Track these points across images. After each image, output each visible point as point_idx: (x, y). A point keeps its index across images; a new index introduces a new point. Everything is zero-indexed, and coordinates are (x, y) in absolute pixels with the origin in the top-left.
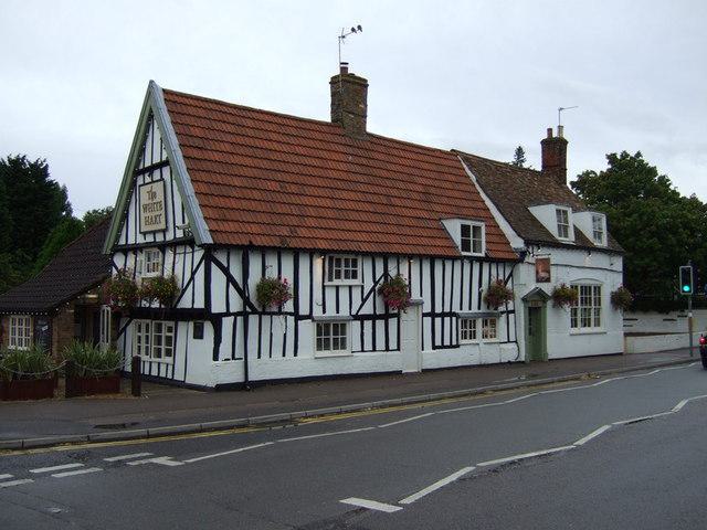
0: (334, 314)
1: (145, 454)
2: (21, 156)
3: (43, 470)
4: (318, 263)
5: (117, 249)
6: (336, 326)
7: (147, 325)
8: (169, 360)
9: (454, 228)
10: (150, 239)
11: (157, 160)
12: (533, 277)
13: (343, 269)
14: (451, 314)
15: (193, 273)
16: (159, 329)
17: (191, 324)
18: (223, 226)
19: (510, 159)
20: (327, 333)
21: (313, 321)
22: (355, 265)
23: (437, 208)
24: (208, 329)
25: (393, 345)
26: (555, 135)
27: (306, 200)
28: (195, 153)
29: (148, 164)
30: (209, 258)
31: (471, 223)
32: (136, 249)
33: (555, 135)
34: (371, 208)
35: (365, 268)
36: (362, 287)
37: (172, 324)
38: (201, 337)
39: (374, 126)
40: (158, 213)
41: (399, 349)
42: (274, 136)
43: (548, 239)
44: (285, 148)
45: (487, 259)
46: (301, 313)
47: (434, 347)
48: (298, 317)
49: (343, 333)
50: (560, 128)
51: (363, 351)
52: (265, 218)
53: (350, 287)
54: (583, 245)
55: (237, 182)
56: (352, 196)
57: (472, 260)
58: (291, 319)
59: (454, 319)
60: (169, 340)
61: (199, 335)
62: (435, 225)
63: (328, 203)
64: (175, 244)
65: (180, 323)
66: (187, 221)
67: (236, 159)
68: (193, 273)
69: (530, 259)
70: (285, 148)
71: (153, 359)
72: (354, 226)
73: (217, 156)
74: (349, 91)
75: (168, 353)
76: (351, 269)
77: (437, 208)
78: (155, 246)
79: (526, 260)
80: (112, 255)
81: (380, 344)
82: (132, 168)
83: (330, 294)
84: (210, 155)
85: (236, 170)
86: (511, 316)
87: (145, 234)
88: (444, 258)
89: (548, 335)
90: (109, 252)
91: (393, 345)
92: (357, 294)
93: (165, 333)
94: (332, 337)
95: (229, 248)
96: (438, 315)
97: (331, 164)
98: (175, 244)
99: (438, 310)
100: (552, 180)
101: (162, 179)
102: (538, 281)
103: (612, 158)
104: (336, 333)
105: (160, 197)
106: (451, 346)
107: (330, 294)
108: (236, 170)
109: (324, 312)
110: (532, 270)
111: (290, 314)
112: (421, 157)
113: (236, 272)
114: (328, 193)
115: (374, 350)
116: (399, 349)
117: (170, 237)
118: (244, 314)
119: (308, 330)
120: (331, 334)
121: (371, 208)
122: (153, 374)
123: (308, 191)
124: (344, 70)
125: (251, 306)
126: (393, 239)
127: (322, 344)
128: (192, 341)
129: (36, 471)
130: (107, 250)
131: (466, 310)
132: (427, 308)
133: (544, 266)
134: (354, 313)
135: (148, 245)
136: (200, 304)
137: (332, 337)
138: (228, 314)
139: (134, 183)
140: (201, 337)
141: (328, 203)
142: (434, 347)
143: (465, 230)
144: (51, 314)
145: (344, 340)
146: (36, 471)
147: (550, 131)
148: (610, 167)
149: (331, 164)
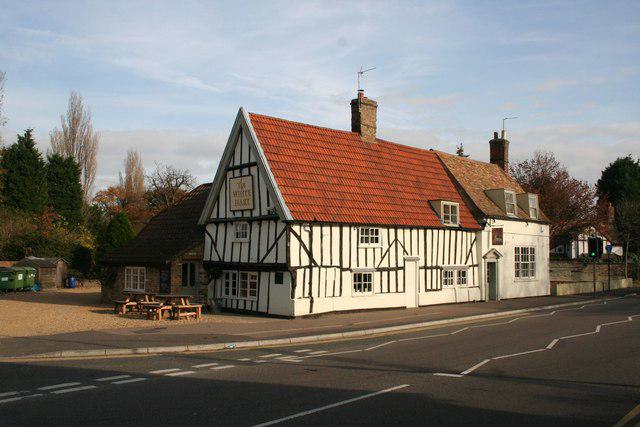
2: (22, 135)
3: (104, 379)
4: (354, 232)
5: (209, 221)
7: (234, 275)
8: (255, 299)
10: (239, 215)
11: (245, 161)
14: (437, 267)
15: (277, 240)
16: (244, 277)
17: (273, 275)
18: (298, 208)
19: (340, 120)
20: (360, 280)
21: (351, 271)
22: (377, 233)
25: (400, 288)
26: (500, 137)
28: (274, 158)
29: (237, 163)
32: (226, 222)
35: (383, 232)
37: (256, 273)
42: (319, 144)
45: (460, 229)
46: (344, 266)
47: (427, 290)
48: (342, 270)
50: (503, 132)
56: (372, 185)
57: (451, 229)
58: (338, 270)
60: (253, 285)
61: (279, 280)
64: (260, 220)
66: (272, 205)
68: (277, 240)
73: (287, 159)
75: (253, 293)
78: (244, 220)
80: (205, 226)
81: (393, 288)
82: (224, 165)
83: (362, 252)
84: (283, 159)
86: (400, 272)
87: (234, 212)
91: (400, 288)
92: (378, 251)
93: (249, 280)
94: (363, 283)
95: (300, 223)
97: (357, 163)
98: (260, 220)
100: (496, 168)
101: (250, 174)
104: (365, 280)
105: (249, 186)
106: (437, 290)
107: (362, 252)
112: (413, 156)
116: (404, 291)
117: (256, 214)
118: (310, 267)
119: (348, 277)
120: (362, 282)
125: (314, 261)
127: (358, 287)
128: (275, 287)
129: (198, 366)
130: (202, 221)
133: (498, 235)
134: (376, 266)
135: (238, 219)
138: (300, 267)
139: (225, 177)
142: (427, 290)
145: (370, 285)
146: (198, 366)
147: (496, 134)
148: (570, 178)
149: (357, 163)
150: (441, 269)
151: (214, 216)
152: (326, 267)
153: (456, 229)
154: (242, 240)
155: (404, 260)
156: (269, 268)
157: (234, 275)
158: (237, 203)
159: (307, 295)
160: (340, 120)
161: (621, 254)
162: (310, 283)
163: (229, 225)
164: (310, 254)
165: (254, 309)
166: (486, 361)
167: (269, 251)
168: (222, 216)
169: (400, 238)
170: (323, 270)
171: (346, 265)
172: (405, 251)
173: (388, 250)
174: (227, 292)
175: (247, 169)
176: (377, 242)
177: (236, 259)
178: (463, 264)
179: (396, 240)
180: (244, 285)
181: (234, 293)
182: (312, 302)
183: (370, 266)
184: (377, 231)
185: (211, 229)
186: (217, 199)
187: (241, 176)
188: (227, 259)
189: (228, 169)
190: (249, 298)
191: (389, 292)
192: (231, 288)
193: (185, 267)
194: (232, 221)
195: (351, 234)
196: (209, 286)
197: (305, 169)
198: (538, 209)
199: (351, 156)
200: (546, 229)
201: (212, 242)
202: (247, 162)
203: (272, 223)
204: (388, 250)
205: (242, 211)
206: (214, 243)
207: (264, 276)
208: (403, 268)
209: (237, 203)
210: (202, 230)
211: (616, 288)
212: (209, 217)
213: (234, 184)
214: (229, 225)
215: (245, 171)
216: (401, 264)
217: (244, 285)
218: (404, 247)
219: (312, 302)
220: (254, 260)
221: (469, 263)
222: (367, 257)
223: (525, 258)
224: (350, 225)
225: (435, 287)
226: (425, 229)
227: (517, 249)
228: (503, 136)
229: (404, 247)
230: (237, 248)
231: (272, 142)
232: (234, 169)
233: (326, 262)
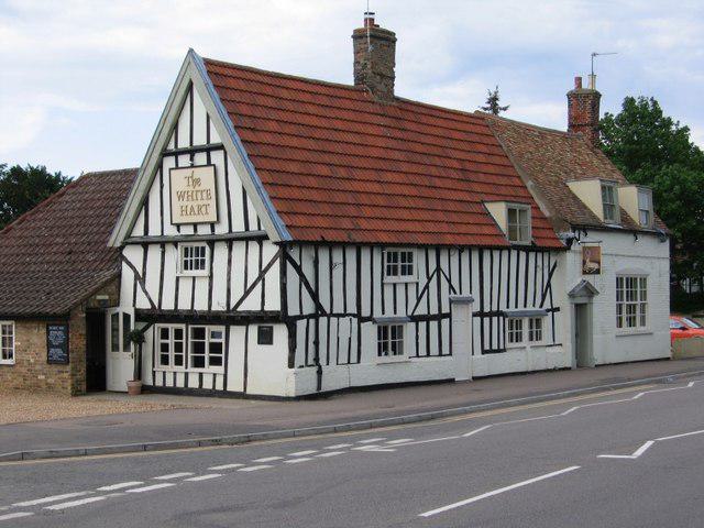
0: (392, 315)
1: (136, 483)
5: (129, 241)
6: (393, 328)
7: (178, 334)
8: (219, 369)
9: (498, 211)
10: (188, 231)
11: (200, 140)
12: (579, 268)
13: (400, 264)
14: (499, 313)
15: (262, 274)
16: (199, 334)
17: (253, 330)
18: (300, 221)
19: (339, 68)
21: (374, 322)
22: (410, 260)
23: (477, 188)
24: (280, 333)
25: (446, 350)
26: (586, 85)
27: (357, 186)
28: (250, 136)
29: (184, 143)
30: (284, 256)
31: (513, 206)
33: (586, 85)
34: (414, 191)
36: (417, 284)
37: (222, 329)
38: (270, 342)
39: (404, 89)
40: (205, 202)
41: (450, 354)
43: (595, 224)
44: (324, 123)
47: (484, 352)
48: (362, 320)
49: (401, 336)
50: (593, 76)
51: (418, 356)
52: (327, 210)
53: (194, 278)
54: (630, 230)
55: (293, 167)
58: (355, 320)
59: (501, 318)
60: (216, 348)
62: (475, 208)
63: (376, 188)
65: (232, 328)
67: (287, 141)
68: (262, 274)
69: (575, 247)
70: (324, 123)
71: (190, 369)
72: (405, 214)
74: (376, 45)
75: (215, 362)
76: (200, 258)
77: (477, 188)
79: (572, 248)
80: (122, 248)
81: (434, 349)
83: (389, 291)
85: (289, 154)
86: (445, 322)
87: (178, 226)
88: (491, 248)
89: (594, 336)
90: (118, 244)
93: (208, 340)
94: (390, 340)
95: (300, 244)
96: (487, 315)
99: (487, 310)
101: (209, 163)
102: (584, 273)
103: (629, 102)
106: (499, 351)
107: (389, 291)
108: (289, 154)
109: (395, 313)
110: (579, 259)
111: (354, 315)
113: (308, 270)
114: (373, 176)
115: (428, 355)
116: (450, 354)
117: (222, 230)
119: (370, 332)
120: (390, 338)
121: (414, 191)
122: (178, 385)
123: (358, 174)
124: (370, 21)
126: (445, 228)
127: (382, 349)
130: (116, 239)
131: (512, 308)
132: (477, 308)
133: (591, 255)
134: (410, 313)
136: (277, 307)
137: (390, 340)
138: (301, 317)
139: (160, 166)
140: (270, 342)
141: (376, 188)
143: (511, 212)
144: (62, 319)
147: (579, 80)
149: (370, 141)
150: (504, 315)
151: (139, 232)
152: (338, 316)
153: (527, 249)
154: (194, 272)
155: (451, 302)
156: (246, 319)
157: (178, 334)
158: (183, 211)
159: (311, 361)
160: (339, 68)
161: (110, 244)
162: (316, 343)
163: (170, 249)
164: (315, 296)
165: (219, 387)
166: (426, 514)
167: (247, 293)
168: (154, 231)
169: (444, 266)
170: (334, 320)
171: (365, 312)
172: (451, 287)
173: (427, 287)
174: (165, 360)
175: (204, 155)
176: (410, 273)
177: (184, 305)
178: (537, 308)
179: (438, 269)
180: (199, 348)
181: (179, 361)
182: (320, 372)
183: (401, 313)
184: (410, 254)
185: (133, 254)
186: (145, 203)
187: (192, 166)
188: (168, 305)
189: (165, 153)
190: (209, 369)
191: (215, 375)
192: (172, 354)
193: (531, 321)
195: (374, 263)
197: (298, 155)
198: (652, 212)
199: (361, 128)
200: (664, 249)
201: (137, 276)
202: (187, 145)
203: (254, 247)
204: (427, 287)
205: (195, 225)
206: (140, 279)
207: (237, 333)
208: (449, 316)
209: (183, 211)
210: (117, 256)
212: (128, 236)
213: (178, 178)
214: (170, 249)
215: (201, 158)
216: (445, 310)
217: (199, 348)
218: (449, 281)
219: (320, 372)
220: (219, 305)
221: (547, 305)
222: (396, 298)
223: (631, 296)
224: (372, 246)
225: (495, 347)
226: (358, 247)
227: (619, 281)
228: (593, 83)
229: (449, 281)
230: (185, 286)
231: (244, 109)
232: (177, 154)
233: (338, 309)
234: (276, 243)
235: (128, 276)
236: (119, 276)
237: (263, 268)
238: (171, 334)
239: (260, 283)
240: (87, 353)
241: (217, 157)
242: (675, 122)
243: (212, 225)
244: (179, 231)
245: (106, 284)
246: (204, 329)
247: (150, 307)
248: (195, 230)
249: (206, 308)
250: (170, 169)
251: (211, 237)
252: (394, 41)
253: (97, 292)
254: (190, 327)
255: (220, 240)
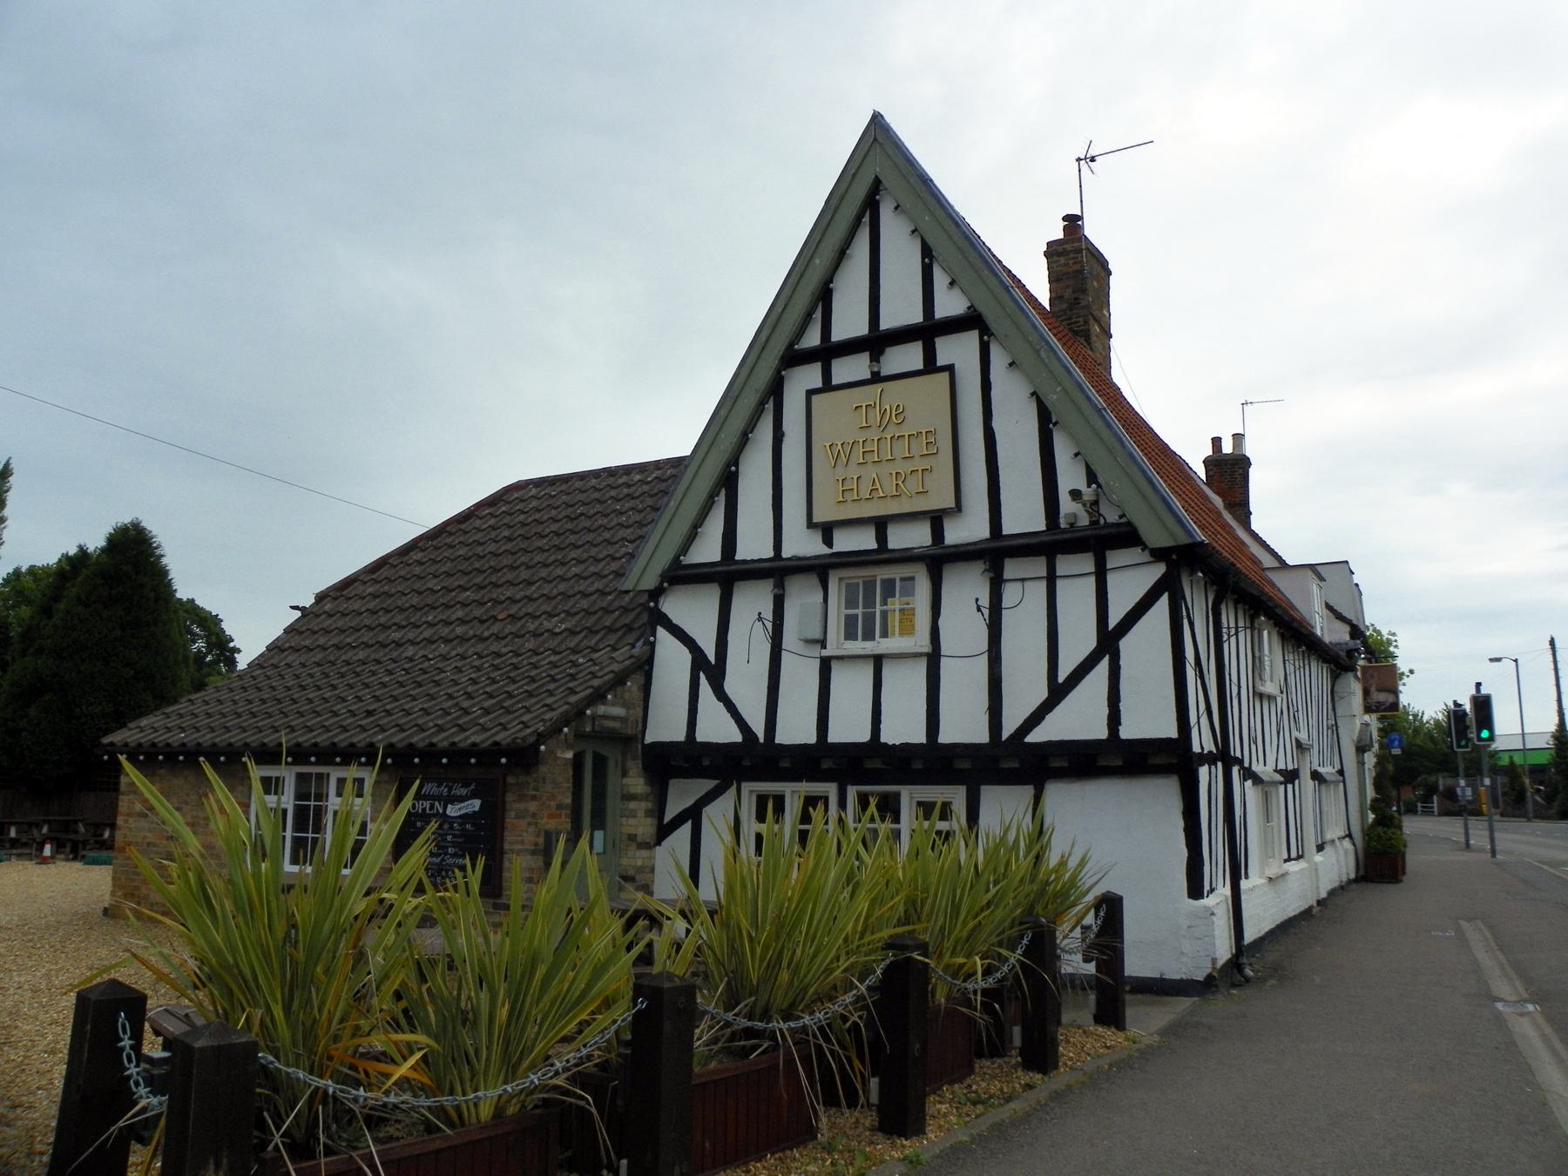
5: (681, 575)
11: (901, 309)
15: (1109, 642)
26: (1227, 448)
37: (957, 796)
39: (883, 740)
53: (878, 661)
80: (656, 594)
87: (827, 531)
90: (650, 582)
139: (776, 390)
167: (1058, 692)
168: (754, 544)
188: (797, 728)
189: (794, 358)
194: (819, 569)
196: (661, 853)
211: (132, 1159)
232: (828, 353)
234: (1159, 555)
235: (672, 660)
236: (645, 666)
237: (1113, 622)
238: (792, 808)
239: (1103, 667)
240: (57, 1145)
241: (952, 349)
242: (1054, 421)
243: (937, 520)
244: (828, 541)
245: (619, 680)
246: (897, 796)
247: (737, 737)
248: (882, 538)
249: (920, 737)
250: (810, 393)
251: (937, 551)
252: (1250, 464)
253: (598, 696)
254: (852, 792)
255: (966, 554)
